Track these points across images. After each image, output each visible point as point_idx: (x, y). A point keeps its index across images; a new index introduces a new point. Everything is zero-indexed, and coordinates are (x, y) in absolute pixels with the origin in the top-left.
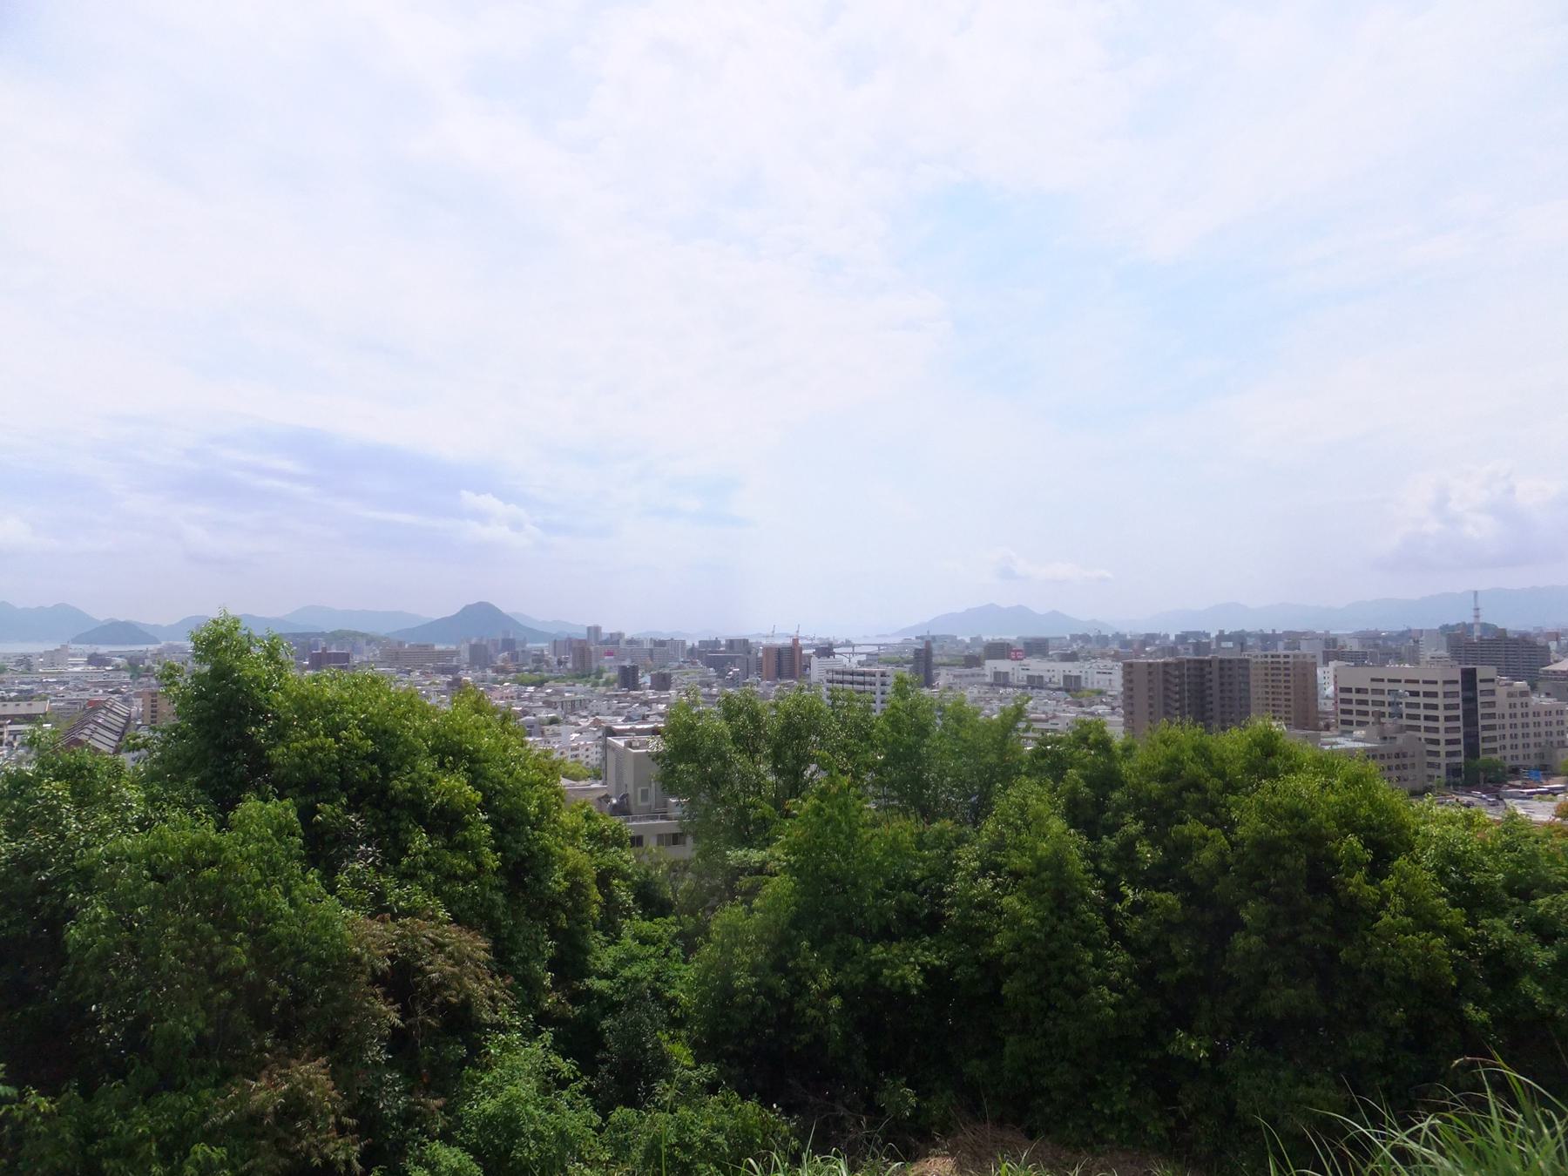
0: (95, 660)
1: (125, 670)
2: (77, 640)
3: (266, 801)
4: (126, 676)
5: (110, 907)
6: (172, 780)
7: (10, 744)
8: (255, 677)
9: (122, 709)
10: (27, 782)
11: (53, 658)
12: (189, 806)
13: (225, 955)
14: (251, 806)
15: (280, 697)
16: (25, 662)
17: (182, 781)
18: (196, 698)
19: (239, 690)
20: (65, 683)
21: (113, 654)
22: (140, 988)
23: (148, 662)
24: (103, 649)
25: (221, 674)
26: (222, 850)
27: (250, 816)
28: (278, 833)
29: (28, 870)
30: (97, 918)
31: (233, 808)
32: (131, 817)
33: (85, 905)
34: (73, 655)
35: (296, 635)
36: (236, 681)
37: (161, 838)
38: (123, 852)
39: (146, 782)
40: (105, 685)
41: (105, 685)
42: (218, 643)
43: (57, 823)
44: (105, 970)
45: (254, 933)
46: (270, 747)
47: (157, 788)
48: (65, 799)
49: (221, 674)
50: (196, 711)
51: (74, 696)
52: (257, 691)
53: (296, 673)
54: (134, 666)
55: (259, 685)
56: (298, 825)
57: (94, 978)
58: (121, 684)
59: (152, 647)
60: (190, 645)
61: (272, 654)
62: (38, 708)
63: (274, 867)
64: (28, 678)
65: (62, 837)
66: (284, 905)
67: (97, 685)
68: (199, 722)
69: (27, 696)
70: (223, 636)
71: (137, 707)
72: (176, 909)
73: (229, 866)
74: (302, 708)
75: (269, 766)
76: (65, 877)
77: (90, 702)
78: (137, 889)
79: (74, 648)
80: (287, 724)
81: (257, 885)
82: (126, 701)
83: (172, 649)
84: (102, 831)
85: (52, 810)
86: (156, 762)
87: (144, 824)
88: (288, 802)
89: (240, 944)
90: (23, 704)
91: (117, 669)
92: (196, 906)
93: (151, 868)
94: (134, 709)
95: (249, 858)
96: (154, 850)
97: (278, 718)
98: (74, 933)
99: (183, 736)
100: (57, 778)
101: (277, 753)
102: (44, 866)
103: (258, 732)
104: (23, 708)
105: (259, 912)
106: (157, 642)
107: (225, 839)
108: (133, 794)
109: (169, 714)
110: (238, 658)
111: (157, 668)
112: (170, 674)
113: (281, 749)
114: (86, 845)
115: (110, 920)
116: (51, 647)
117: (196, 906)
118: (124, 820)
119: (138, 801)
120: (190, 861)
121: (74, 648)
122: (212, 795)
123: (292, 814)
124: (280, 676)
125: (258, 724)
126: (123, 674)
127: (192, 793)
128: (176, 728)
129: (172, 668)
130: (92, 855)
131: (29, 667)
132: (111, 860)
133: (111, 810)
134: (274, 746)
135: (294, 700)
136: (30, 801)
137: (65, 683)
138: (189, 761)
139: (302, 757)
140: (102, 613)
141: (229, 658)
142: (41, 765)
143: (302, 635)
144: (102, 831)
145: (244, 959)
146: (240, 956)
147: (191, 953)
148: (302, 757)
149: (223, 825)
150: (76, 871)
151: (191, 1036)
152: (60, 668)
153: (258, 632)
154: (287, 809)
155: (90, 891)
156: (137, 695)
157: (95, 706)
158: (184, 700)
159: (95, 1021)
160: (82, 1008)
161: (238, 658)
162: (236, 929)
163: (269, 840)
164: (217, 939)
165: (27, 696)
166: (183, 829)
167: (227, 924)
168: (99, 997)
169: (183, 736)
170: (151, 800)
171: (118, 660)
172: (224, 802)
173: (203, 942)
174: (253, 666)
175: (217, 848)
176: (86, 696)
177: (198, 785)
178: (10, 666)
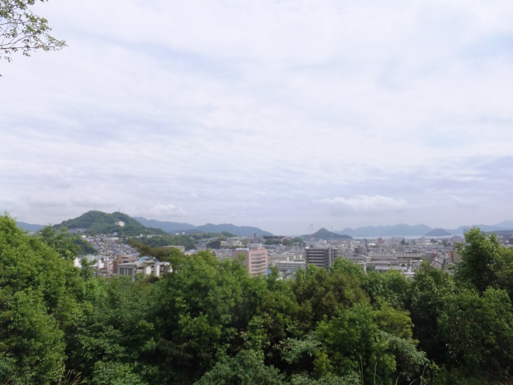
0: (433, 241)
1: (442, 244)
2: (428, 234)
3: (496, 289)
4: (442, 246)
5: (449, 315)
6: (463, 279)
7: (412, 266)
8: (487, 248)
9: (442, 256)
10: (422, 276)
11: (421, 240)
12: (469, 288)
13: (487, 338)
14: (490, 290)
15: (497, 254)
16: (414, 242)
17: (466, 280)
18: (468, 254)
19: (482, 252)
20: (425, 248)
21: (438, 239)
22: (460, 342)
23: (449, 242)
24: (435, 238)
25: (475, 247)
26: (482, 304)
27: (491, 294)
28: (502, 300)
29: (425, 301)
30: (445, 318)
31: (484, 290)
32: (452, 289)
33: (442, 313)
34: (426, 240)
35: (501, 231)
36: (481, 249)
37: (462, 296)
38: (450, 300)
39: (455, 279)
40: (437, 249)
41: (437, 249)
42: (474, 237)
43: (431, 288)
44: (449, 334)
45: (497, 334)
46: (495, 271)
47: (458, 281)
48: (432, 282)
49: (475, 247)
50: (468, 258)
51: (428, 252)
52: (488, 252)
53: (503, 245)
54: (445, 243)
55: (489, 250)
56: (509, 299)
57: (446, 335)
58: (441, 248)
59: (450, 237)
60: (463, 237)
61: (493, 240)
62: (418, 255)
63: (501, 312)
64: (415, 246)
65: (433, 292)
66: (507, 326)
67: (434, 249)
68: (469, 262)
69: (415, 252)
70: (474, 234)
71: (447, 256)
72: (469, 320)
73: (485, 309)
74: (506, 259)
75: (496, 278)
76: (435, 304)
77: (433, 254)
78: (456, 311)
79: (426, 237)
80: (501, 264)
81: (496, 317)
82: (443, 254)
83: (456, 237)
84: (444, 292)
85: (430, 284)
86: (458, 273)
87: (456, 292)
88: (504, 291)
89: (492, 335)
90: (414, 254)
91: (439, 244)
92: (475, 320)
93: (459, 305)
94: (446, 257)
95: (492, 308)
96: (460, 300)
97: (497, 261)
98: (439, 321)
99: (465, 266)
100: (430, 275)
101: (499, 273)
102: (430, 300)
103: (491, 266)
104: (415, 255)
105: (497, 326)
106: (451, 235)
107: (483, 300)
108: (452, 283)
109: (459, 259)
110: (481, 241)
111: (452, 243)
112: (458, 246)
113: (500, 272)
114: (440, 296)
115: (449, 319)
116: (420, 237)
117: (475, 320)
118: (450, 290)
119: (453, 285)
120: (472, 305)
121: (426, 237)
122: (477, 285)
123: (507, 295)
124: (497, 247)
125: (490, 263)
126: (441, 245)
127: (470, 284)
128: (462, 263)
129: (459, 244)
130: (441, 299)
131: (415, 244)
132: (447, 301)
133: (446, 286)
134: (497, 271)
135: (503, 256)
136: (424, 281)
137: (425, 248)
138: (468, 274)
139: (508, 275)
140: (434, 226)
141: (477, 241)
142: (426, 272)
143: (505, 231)
144: (444, 292)
145: (494, 341)
146: (492, 339)
147: (475, 335)
148: (508, 275)
149: (481, 295)
150: (438, 303)
151: (478, 361)
152: (423, 243)
153: (486, 231)
154: (504, 293)
155: (443, 310)
156: (447, 252)
157: (434, 256)
158: (464, 254)
159: (447, 349)
160: (443, 344)
161: (481, 241)
162: (490, 331)
163: (499, 303)
164: (484, 332)
165: (415, 252)
166: (469, 295)
167: (487, 328)
168: (448, 342)
169: (465, 266)
170: (457, 285)
171: (440, 241)
172: (481, 288)
173: (479, 332)
174: (487, 243)
175: (480, 302)
176: (431, 252)
177: (471, 282)
178: (410, 242)
